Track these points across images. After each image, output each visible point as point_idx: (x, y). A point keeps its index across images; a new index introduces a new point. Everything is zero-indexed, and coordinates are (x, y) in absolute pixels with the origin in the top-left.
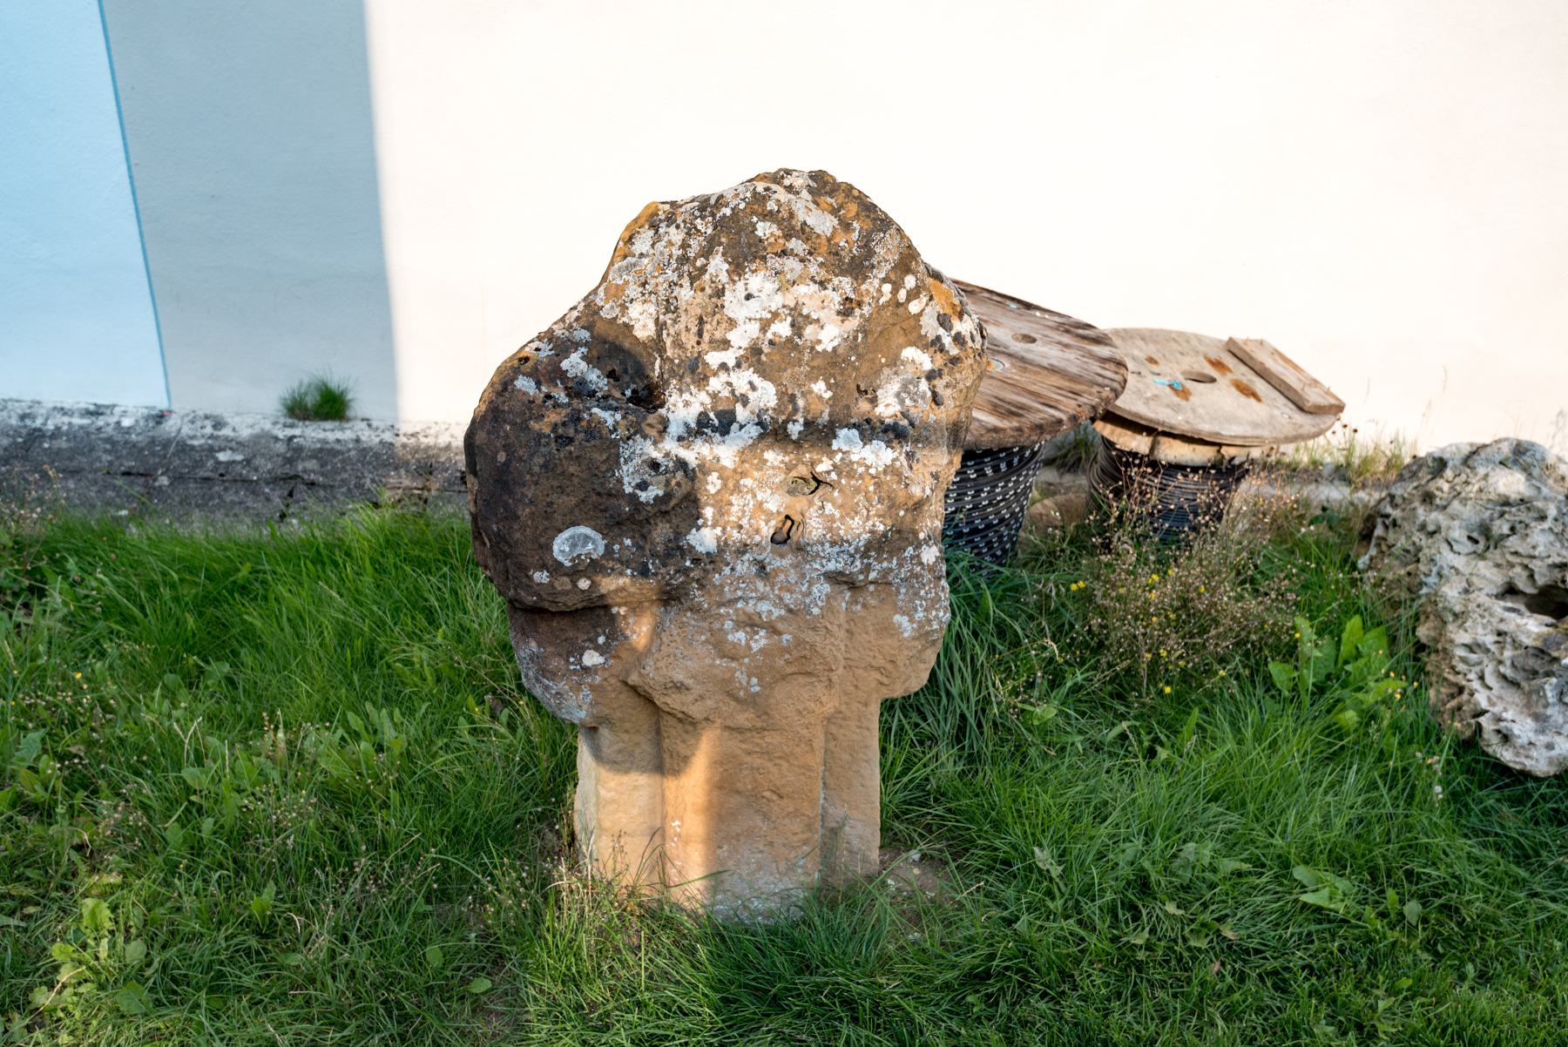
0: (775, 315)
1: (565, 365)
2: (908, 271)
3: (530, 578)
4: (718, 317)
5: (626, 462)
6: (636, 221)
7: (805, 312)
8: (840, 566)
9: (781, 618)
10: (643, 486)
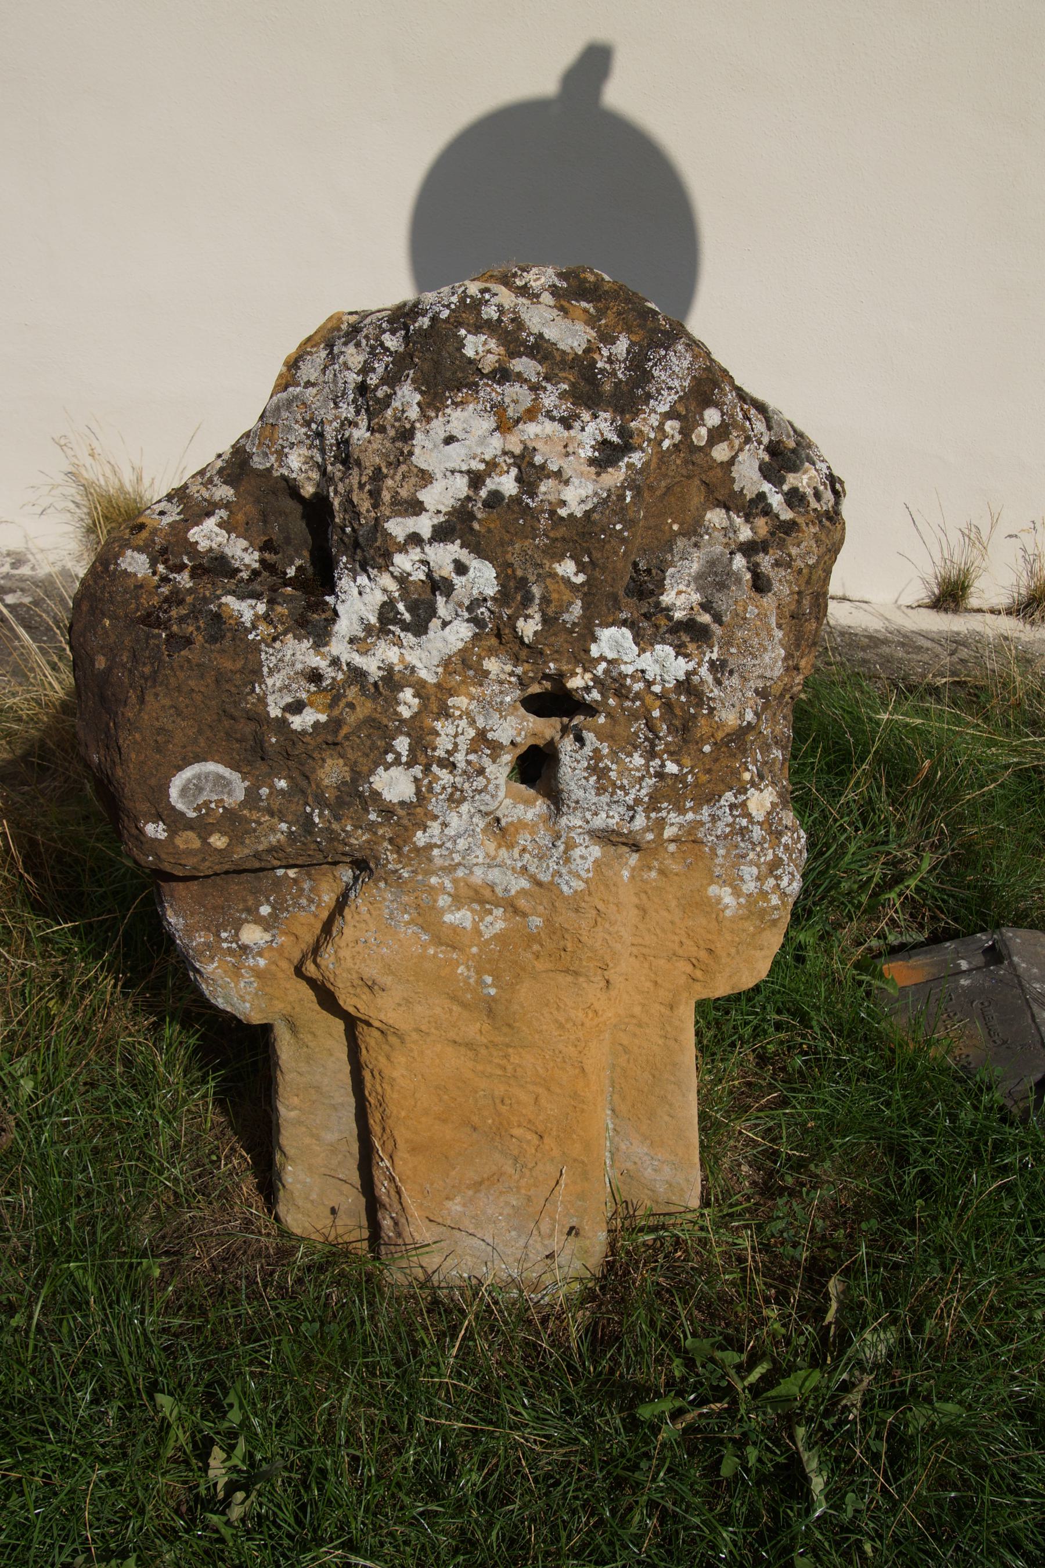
0: (492, 466)
1: (195, 534)
2: (707, 402)
3: (141, 831)
4: (403, 468)
5: (271, 672)
6: (309, 339)
7: (538, 460)
8: (612, 823)
9: (523, 892)
10: (296, 708)
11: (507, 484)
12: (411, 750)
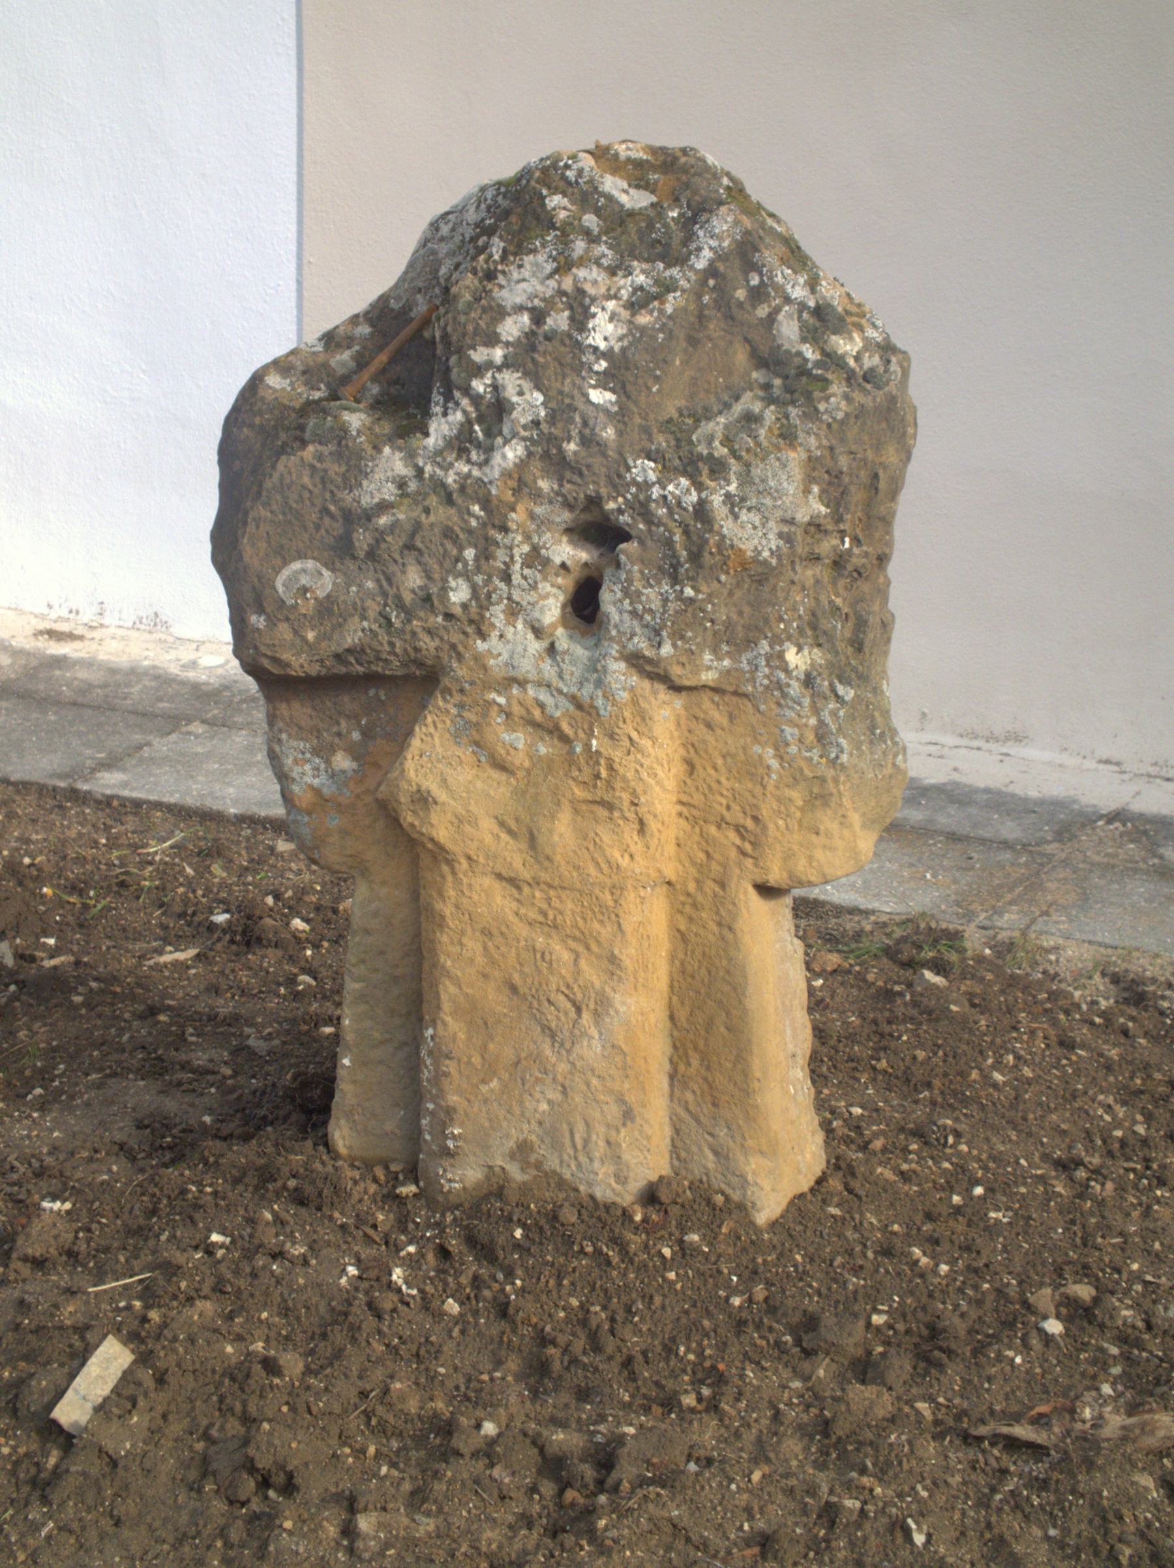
0: (550, 302)
11: (559, 320)
12: (477, 559)
